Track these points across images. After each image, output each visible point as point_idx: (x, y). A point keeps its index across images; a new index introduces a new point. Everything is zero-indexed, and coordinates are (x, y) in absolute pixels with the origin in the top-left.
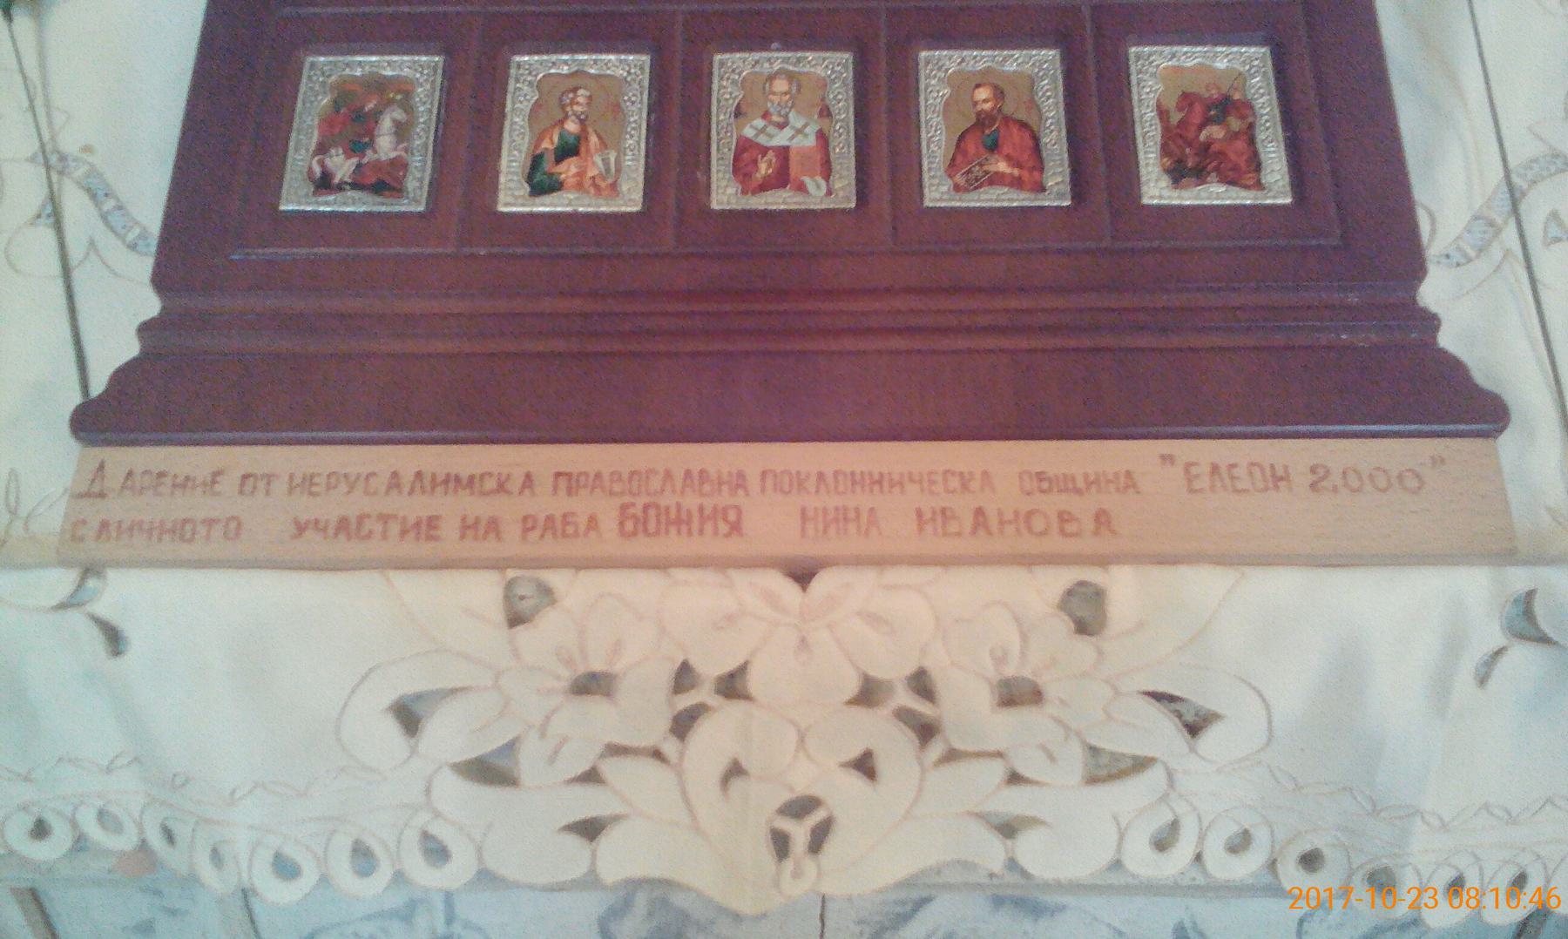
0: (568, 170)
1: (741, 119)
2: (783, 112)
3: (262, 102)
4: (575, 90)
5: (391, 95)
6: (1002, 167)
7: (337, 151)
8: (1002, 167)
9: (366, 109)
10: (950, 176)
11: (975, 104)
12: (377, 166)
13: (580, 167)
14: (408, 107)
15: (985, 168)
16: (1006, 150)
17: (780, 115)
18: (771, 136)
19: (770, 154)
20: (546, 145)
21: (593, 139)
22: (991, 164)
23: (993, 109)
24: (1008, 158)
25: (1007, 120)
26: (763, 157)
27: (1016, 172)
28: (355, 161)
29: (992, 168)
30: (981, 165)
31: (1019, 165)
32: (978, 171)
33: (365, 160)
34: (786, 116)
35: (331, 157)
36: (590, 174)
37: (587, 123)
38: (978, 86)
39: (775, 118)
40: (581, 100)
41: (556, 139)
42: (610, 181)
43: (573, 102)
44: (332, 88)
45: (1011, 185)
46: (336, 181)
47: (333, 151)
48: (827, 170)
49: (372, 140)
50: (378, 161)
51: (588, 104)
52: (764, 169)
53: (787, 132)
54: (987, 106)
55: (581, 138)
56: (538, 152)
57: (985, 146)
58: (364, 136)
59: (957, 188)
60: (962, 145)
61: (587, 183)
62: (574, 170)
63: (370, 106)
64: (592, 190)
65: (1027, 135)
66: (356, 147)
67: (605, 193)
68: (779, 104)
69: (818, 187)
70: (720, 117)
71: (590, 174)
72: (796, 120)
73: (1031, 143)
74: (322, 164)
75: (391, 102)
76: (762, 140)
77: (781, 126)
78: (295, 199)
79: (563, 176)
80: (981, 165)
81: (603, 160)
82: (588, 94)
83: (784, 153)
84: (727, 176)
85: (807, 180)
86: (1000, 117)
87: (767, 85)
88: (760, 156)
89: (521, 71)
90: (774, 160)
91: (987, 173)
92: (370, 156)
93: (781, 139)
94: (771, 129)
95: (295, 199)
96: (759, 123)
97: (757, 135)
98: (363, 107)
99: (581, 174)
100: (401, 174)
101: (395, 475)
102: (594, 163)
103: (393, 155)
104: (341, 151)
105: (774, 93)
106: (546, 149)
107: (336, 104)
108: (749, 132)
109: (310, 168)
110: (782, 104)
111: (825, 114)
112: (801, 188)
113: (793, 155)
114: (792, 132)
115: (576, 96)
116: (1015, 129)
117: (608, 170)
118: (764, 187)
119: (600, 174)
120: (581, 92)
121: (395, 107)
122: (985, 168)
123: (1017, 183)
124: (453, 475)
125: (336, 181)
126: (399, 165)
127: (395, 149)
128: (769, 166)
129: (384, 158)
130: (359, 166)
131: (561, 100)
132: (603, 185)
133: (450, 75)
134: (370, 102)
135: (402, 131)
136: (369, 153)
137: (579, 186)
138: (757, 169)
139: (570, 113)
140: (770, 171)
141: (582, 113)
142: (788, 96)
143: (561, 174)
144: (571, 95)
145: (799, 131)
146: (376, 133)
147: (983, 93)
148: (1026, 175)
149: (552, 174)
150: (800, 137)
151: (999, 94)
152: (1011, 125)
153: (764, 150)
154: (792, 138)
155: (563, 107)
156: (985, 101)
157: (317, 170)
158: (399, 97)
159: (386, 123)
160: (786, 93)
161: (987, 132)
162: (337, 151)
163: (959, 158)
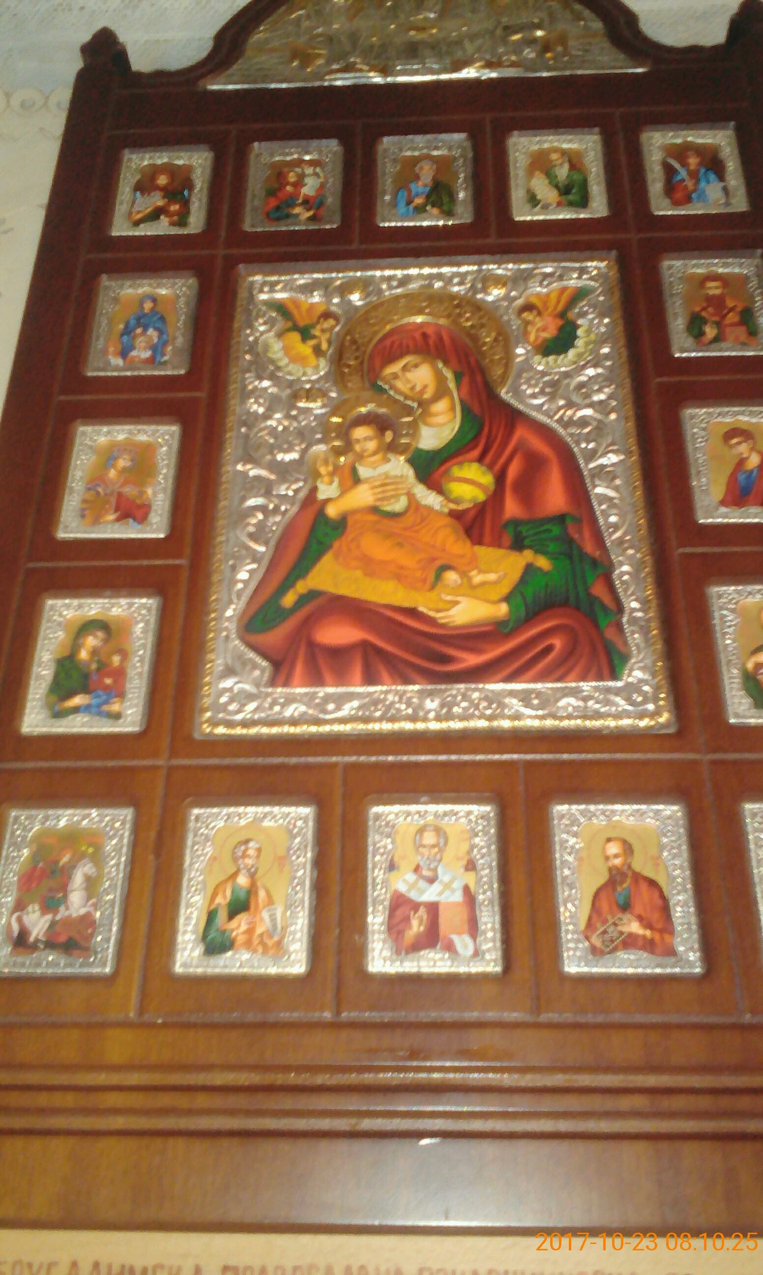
0: (239, 926)
1: (394, 874)
2: (432, 866)
3: (73, 24)
4: (247, 842)
5: (84, 848)
6: (635, 927)
7: (33, 908)
8: (635, 927)
9: (61, 863)
10: (587, 938)
11: (607, 858)
12: (68, 922)
13: (249, 924)
14: (98, 859)
15: (620, 928)
16: (638, 909)
17: (429, 869)
18: (422, 892)
19: (422, 911)
20: (219, 900)
21: (262, 894)
22: (624, 924)
23: (623, 865)
24: (640, 918)
25: (637, 877)
26: (415, 913)
27: (648, 933)
28: (49, 917)
29: (626, 929)
30: (615, 924)
31: (649, 926)
32: (613, 932)
33: (58, 917)
34: (435, 870)
35: (28, 914)
36: (259, 931)
37: (257, 876)
38: (609, 840)
39: (426, 873)
40: (251, 852)
41: (228, 893)
42: (276, 938)
43: (244, 855)
44: (32, 841)
45: (643, 948)
46: (32, 939)
47: (30, 908)
48: (473, 928)
49: (65, 897)
50: (70, 916)
51: (258, 857)
52: (416, 926)
53: (436, 887)
54: (618, 862)
55: (252, 891)
56: (212, 907)
57: (618, 905)
58: (58, 891)
59: (594, 951)
60: (597, 904)
61: (256, 941)
62: (244, 927)
63: (65, 859)
64: (260, 949)
65: (656, 895)
66: (49, 905)
67: (271, 952)
68: (428, 858)
69: (466, 947)
70: (376, 874)
71: (259, 931)
72: (444, 876)
73: (659, 902)
74: (20, 920)
75: (83, 856)
76: (413, 895)
77: (431, 881)
78: (120, 229)
79: (234, 934)
80: (615, 924)
81: (270, 916)
82: (257, 846)
83: (433, 908)
84: (382, 936)
85: (455, 938)
86: (630, 874)
87: (418, 838)
88: (412, 913)
89: (199, 825)
90: (425, 917)
91: (621, 933)
92: (62, 913)
93: (430, 895)
94: (422, 884)
95: (120, 229)
96: (411, 877)
97: (409, 890)
98: (57, 862)
99: (250, 931)
100: (90, 931)
101: (74, 1264)
102: (262, 919)
103: (83, 911)
104: (37, 907)
105: (424, 846)
106: (219, 904)
107: (35, 857)
108: (402, 888)
109: (9, 924)
110: (431, 857)
111: (470, 867)
112: (450, 948)
113: (442, 910)
114: (440, 888)
115: (246, 849)
116: (644, 887)
117: (275, 926)
118: (416, 947)
119: (268, 931)
120: (251, 844)
121: (85, 861)
122: (620, 928)
123: (649, 946)
124: (127, 1267)
125: (32, 939)
126: (87, 921)
127: (85, 906)
128: (420, 924)
129: (74, 915)
130: (53, 924)
131: (234, 853)
132: (270, 943)
133: (137, 829)
134: (64, 855)
135: (91, 885)
136: (62, 909)
137: (248, 945)
138: (410, 927)
139: (242, 866)
140: (422, 928)
141: (253, 866)
142: (436, 850)
143: (233, 931)
144: (243, 848)
145: (447, 886)
146: (69, 889)
147: (613, 849)
148: (657, 937)
149: (224, 932)
150: (447, 893)
151: (628, 848)
152: (641, 882)
153: (416, 906)
154: (440, 894)
155: (235, 859)
156: (616, 856)
157: (16, 928)
158: (91, 850)
159: (78, 879)
160: (434, 846)
161: (619, 889)
162: (33, 908)
163: (595, 918)
